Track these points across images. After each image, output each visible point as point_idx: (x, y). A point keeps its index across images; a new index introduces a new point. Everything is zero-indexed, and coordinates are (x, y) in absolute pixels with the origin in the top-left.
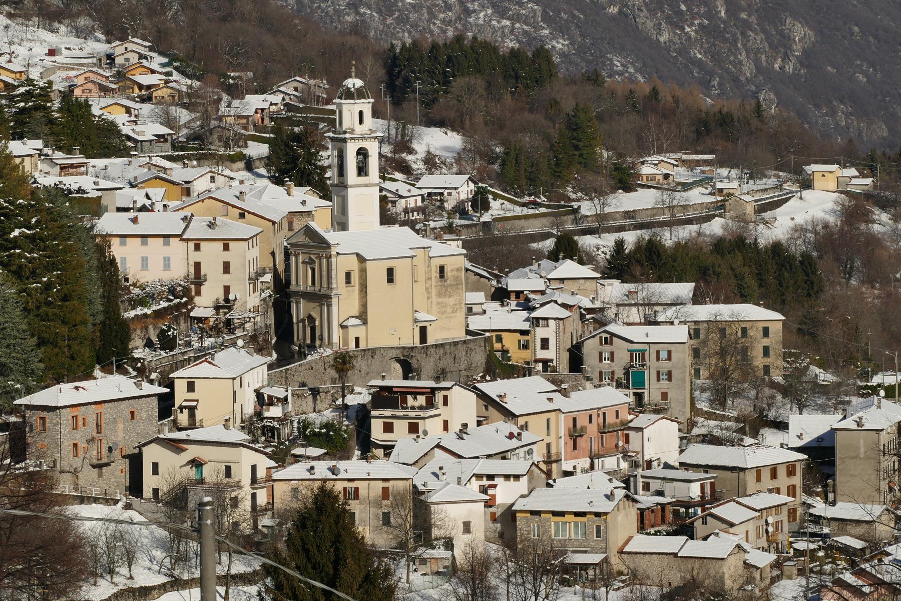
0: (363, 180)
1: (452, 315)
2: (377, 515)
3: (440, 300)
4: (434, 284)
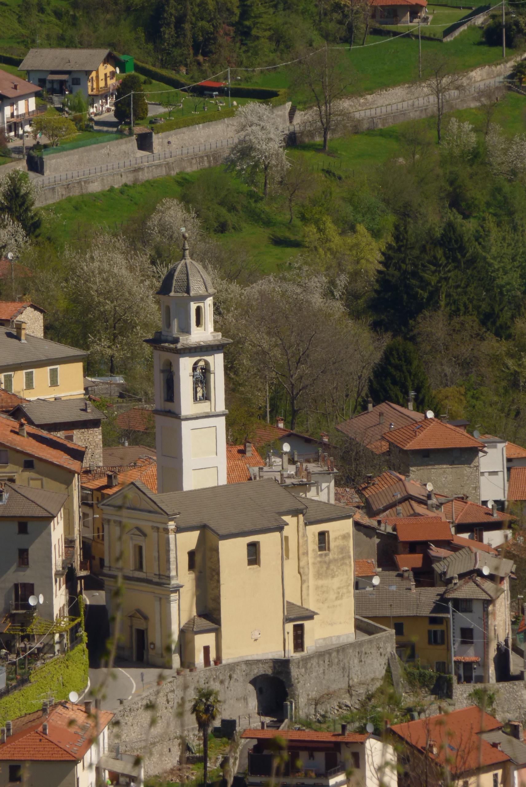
0: (204, 407)
1: (338, 602)
2: (223, 712)
3: (320, 582)
4: (311, 561)
